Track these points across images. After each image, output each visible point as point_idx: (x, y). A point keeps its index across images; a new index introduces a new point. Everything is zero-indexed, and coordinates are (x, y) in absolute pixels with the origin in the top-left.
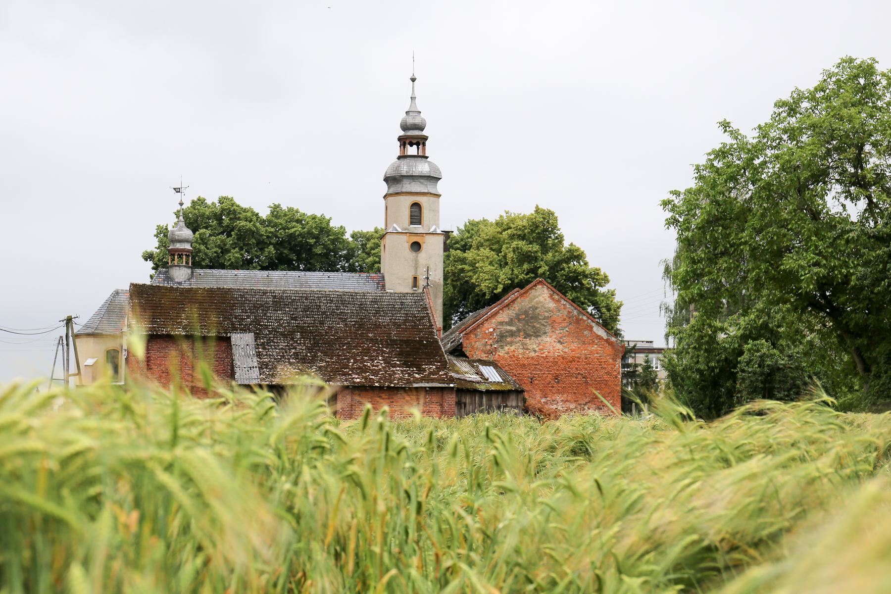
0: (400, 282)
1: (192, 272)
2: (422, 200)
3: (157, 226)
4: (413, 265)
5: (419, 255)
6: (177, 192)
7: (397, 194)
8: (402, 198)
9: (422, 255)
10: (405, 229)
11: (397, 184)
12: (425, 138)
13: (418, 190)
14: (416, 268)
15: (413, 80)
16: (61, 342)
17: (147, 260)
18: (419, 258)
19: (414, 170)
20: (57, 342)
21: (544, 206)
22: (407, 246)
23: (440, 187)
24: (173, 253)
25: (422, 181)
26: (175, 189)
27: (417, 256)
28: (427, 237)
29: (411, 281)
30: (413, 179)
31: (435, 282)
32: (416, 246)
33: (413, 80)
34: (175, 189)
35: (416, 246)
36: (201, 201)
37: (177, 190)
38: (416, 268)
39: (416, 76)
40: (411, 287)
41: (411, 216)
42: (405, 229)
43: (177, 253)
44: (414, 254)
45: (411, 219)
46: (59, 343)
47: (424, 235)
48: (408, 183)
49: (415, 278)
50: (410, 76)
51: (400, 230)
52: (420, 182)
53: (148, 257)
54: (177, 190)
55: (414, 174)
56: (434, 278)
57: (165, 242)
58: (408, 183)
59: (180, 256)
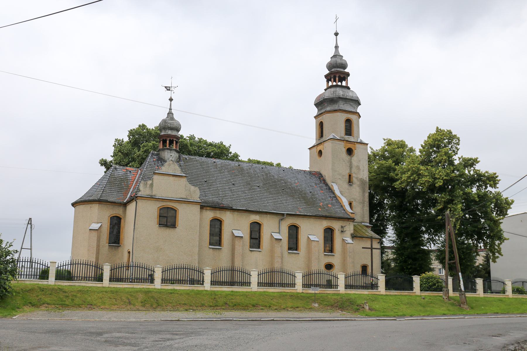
0: (340, 177)
1: (179, 157)
2: (353, 117)
3: (116, 139)
4: (349, 165)
5: (353, 158)
6: (168, 90)
7: (336, 111)
8: (339, 114)
9: (355, 159)
10: (342, 138)
11: (334, 104)
12: (348, 74)
13: (350, 110)
14: (351, 168)
15: (336, 34)
16: (30, 222)
17: (102, 166)
18: (352, 161)
19: (347, 94)
20: (28, 222)
21: (395, 138)
22: (344, 150)
23: (359, 110)
24: (164, 138)
25: (352, 103)
26: (166, 87)
27: (351, 159)
28: (358, 145)
29: (347, 177)
30: (346, 101)
31: (363, 180)
32: (350, 152)
33: (336, 34)
34: (166, 87)
35: (350, 152)
36: (143, 126)
37: (168, 89)
38: (351, 167)
39: (338, 32)
40: (347, 182)
41: (346, 129)
42: (342, 138)
43: (168, 139)
44: (349, 157)
45: (346, 131)
46: (28, 223)
47: (356, 143)
48: (342, 104)
49: (350, 175)
50: (335, 32)
51: (339, 138)
52: (350, 104)
53: (104, 163)
54: (168, 89)
55: (347, 98)
56: (363, 177)
57: (123, 150)
58: (342, 104)
59: (171, 142)
